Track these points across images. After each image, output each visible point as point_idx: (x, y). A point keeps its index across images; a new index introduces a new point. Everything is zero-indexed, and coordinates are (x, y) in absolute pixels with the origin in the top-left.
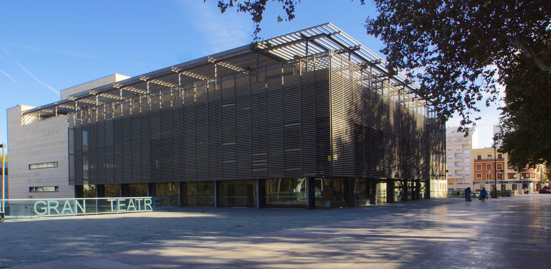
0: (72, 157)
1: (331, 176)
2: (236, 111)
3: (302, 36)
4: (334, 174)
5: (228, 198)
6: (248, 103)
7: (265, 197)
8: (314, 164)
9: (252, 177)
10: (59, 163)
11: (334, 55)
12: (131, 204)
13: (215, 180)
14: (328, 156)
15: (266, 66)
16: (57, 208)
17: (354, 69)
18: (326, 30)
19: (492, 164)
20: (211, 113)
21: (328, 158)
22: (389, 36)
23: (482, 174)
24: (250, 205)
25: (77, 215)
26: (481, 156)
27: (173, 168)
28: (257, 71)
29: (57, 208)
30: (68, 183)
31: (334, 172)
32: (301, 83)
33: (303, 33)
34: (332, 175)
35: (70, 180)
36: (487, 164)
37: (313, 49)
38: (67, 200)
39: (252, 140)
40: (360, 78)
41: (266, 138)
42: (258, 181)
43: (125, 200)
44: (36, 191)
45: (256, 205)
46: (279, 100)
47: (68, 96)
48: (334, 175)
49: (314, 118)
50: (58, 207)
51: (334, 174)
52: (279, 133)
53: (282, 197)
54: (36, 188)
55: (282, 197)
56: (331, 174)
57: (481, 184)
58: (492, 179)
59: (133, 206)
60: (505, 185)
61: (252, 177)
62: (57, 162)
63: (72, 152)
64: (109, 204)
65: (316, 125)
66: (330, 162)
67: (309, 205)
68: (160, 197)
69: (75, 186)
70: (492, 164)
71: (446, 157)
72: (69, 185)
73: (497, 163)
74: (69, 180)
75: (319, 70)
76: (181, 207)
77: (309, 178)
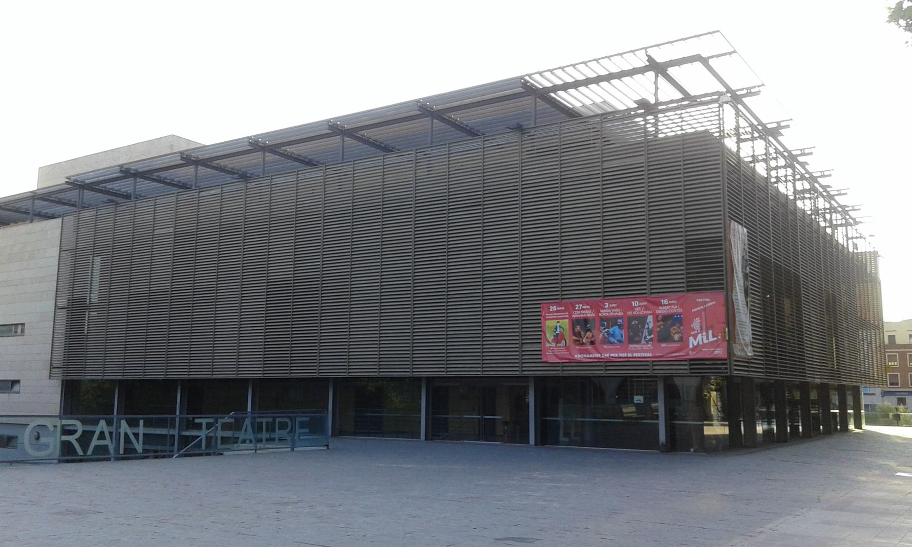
1: (729, 374)
2: (485, 217)
3: (650, 59)
5: (447, 415)
10: (26, 326)
15: (561, 123)
16: (76, 440)
18: (702, 48)
19: (897, 354)
23: (899, 374)
24: (518, 435)
26: (894, 336)
27: (169, 343)
28: (533, 135)
29: (76, 440)
30: (47, 373)
31: (735, 365)
32: (325, 191)
33: (651, 52)
35: (52, 367)
36: (908, 354)
41: (558, 279)
46: (227, 224)
48: (735, 372)
49: (682, 240)
56: (728, 371)
57: (899, 395)
58: (899, 386)
60: (905, 399)
62: (23, 324)
63: (63, 302)
65: (687, 256)
67: (666, 442)
68: (310, 415)
69: (63, 381)
70: (897, 354)
71: (883, 336)
72: (50, 378)
73: (888, 352)
74: (51, 365)
75: (666, 138)
76: (332, 436)
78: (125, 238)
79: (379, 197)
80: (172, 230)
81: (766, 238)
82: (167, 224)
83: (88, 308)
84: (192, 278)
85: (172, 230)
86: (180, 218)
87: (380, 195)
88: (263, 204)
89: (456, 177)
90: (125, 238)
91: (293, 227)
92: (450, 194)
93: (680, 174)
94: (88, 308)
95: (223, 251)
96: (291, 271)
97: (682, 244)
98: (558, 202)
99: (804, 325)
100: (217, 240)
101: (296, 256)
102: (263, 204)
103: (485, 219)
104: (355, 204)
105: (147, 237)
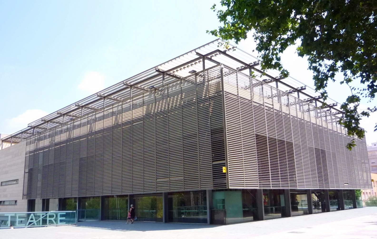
0: (27, 175)
3: (158, 71)
4: (230, 186)
6: (196, 131)
7: (172, 211)
8: (167, 170)
9: (157, 191)
11: (224, 67)
12: (32, 219)
13: (129, 194)
14: (222, 168)
17: (230, 72)
20: (129, 131)
21: (222, 170)
22: (246, 20)
25: (42, 227)
34: (228, 187)
37: (208, 64)
38: (32, 213)
39: (156, 153)
40: (249, 86)
42: (163, 195)
43: (65, 213)
44: (4, 204)
45: (8, 224)
47: (375, 193)
50: (55, 218)
51: (230, 186)
52: (128, 134)
53: (196, 211)
54: (4, 202)
55: (196, 211)
59: (34, 221)
61: (157, 191)
64: (246, 214)
66: (225, 173)
74: (23, 194)
77: (209, 190)
78: (74, 181)
79: (181, 122)
80: (182, 178)
81: (280, 118)
82: (204, 179)
83: (102, 160)
84: (111, 165)
85: (182, 178)
86: (82, 149)
87: (181, 121)
88: (129, 140)
89: (177, 120)
90: (74, 181)
91: (181, 141)
92: (183, 126)
93: (93, 170)
94: (102, 160)
95: (105, 164)
96: (142, 163)
97: (210, 139)
98: (131, 156)
99: (255, 143)
100: (111, 165)
101: (184, 156)
102: (129, 140)
103: (133, 157)
104: (183, 124)
105: (159, 127)
